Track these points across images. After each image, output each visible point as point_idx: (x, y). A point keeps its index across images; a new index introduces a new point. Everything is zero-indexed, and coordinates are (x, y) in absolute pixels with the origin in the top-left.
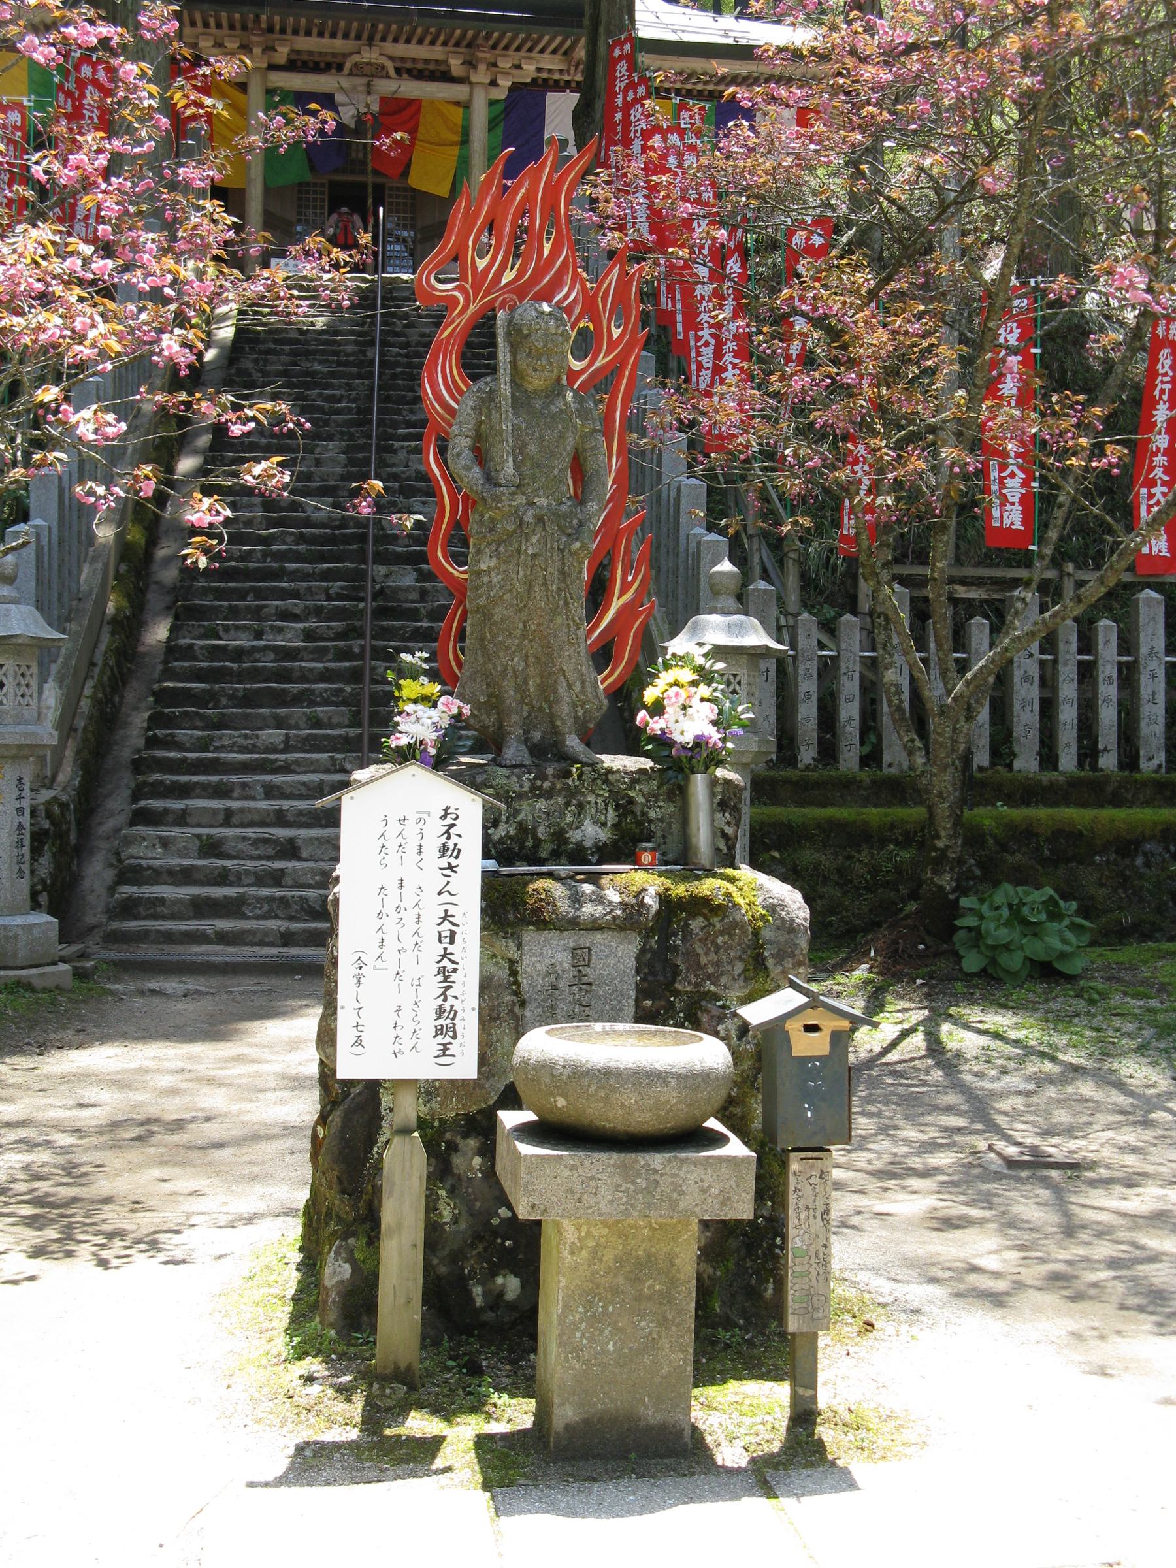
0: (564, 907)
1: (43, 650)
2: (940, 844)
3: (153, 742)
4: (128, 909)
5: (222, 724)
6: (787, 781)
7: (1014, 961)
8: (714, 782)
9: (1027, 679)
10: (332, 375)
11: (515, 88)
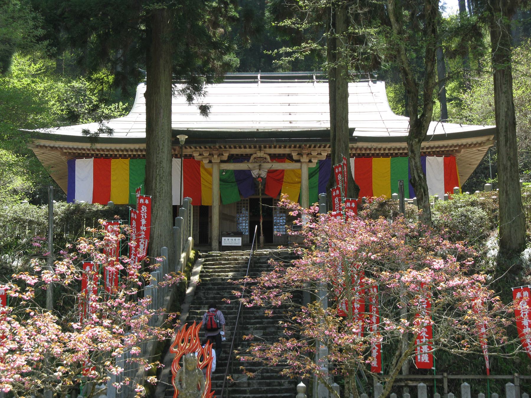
11: (320, 162)
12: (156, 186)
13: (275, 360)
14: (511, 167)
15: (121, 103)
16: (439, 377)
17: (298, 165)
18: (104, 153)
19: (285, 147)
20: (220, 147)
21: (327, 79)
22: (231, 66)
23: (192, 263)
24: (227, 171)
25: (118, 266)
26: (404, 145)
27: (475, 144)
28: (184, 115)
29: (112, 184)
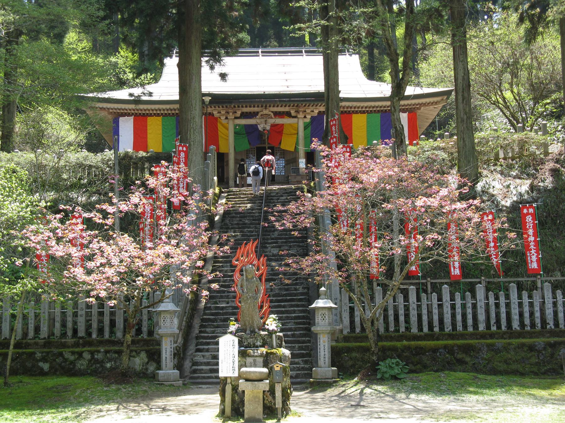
0: (252, 354)
1: (175, 312)
2: (372, 350)
3: (201, 332)
4: (195, 371)
5: (218, 327)
6: (352, 337)
7: (387, 376)
8: (276, 336)
9: (414, 309)
10: (251, 224)
11: (313, 118)
12: (190, 137)
13: (308, 270)
14: (467, 119)
15: (149, 74)
16: (424, 281)
17: (296, 120)
18: (141, 112)
19: (285, 106)
20: (235, 107)
21: (321, 53)
22: (244, 42)
23: (218, 197)
24: (239, 125)
25: (180, 198)
26: (388, 103)
27: (432, 103)
28: (210, 82)
29: (149, 136)
